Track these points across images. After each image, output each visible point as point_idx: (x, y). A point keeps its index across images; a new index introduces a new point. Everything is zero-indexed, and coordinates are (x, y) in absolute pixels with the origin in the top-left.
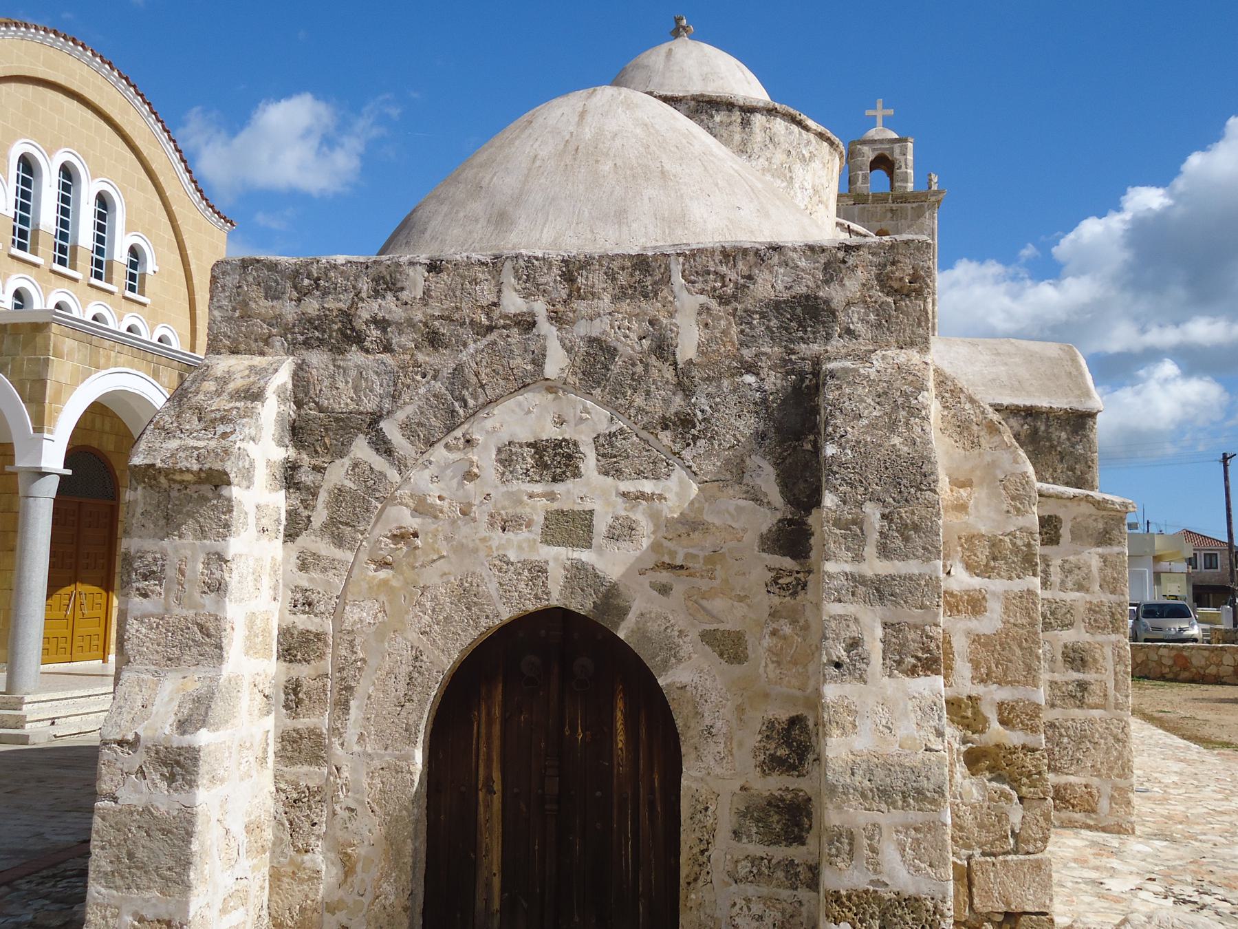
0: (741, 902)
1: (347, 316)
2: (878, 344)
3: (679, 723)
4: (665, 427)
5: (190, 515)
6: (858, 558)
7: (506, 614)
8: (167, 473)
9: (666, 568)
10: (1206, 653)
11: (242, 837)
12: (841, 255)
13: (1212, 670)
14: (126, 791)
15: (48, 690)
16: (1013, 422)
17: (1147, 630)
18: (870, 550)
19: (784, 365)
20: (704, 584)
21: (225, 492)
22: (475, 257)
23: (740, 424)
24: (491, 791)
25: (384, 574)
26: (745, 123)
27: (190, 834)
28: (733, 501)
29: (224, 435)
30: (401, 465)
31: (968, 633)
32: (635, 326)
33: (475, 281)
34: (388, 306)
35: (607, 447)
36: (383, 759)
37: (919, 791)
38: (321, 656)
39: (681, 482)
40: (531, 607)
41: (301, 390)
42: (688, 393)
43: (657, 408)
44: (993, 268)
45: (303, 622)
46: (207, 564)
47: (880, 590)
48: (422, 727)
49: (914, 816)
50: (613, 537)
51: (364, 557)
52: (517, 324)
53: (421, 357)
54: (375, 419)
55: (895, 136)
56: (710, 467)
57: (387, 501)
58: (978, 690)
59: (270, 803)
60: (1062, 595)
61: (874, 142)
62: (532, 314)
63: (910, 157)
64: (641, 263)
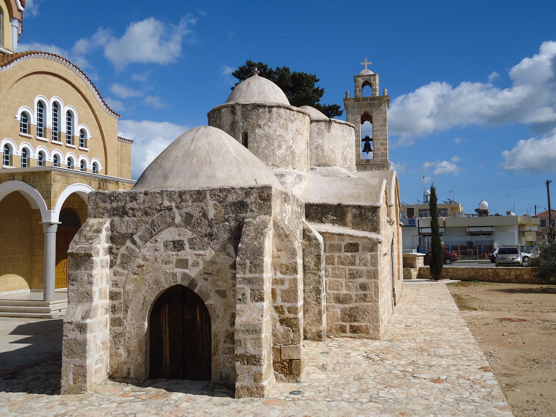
0: (226, 359)
1: (124, 207)
2: (259, 214)
3: (210, 314)
4: (206, 237)
5: (83, 264)
6: (244, 273)
7: (167, 286)
8: (77, 254)
9: (206, 273)
10: (505, 271)
11: (101, 345)
12: (249, 190)
13: (507, 277)
14: (70, 334)
15: (58, 299)
16: (354, 210)
17: (499, 259)
18: (247, 271)
19: (236, 219)
20: (216, 278)
21: (91, 258)
22: (156, 191)
23: (225, 235)
24: (166, 332)
25: (135, 276)
26: (270, 112)
27: (86, 345)
28: (223, 256)
29: (91, 243)
30: (139, 247)
31: (280, 289)
32: (198, 209)
33: (156, 198)
34: (134, 204)
35: (191, 241)
36: (138, 325)
37: (255, 330)
38: (120, 298)
39: (210, 251)
40: (173, 284)
41: (113, 227)
42: (211, 227)
43: (204, 231)
44: (478, 85)
45: (115, 289)
46: (88, 277)
47: (249, 281)
48: (147, 316)
49: (254, 336)
50: (193, 266)
51: (130, 272)
52: (168, 209)
53: (143, 218)
54: (132, 234)
55: (373, 73)
56: (217, 247)
57: (136, 257)
58: (283, 304)
59: (109, 337)
60: (359, 268)
61: (363, 76)
62: (171, 206)
63: (377, 82)
64: (199, 192)
